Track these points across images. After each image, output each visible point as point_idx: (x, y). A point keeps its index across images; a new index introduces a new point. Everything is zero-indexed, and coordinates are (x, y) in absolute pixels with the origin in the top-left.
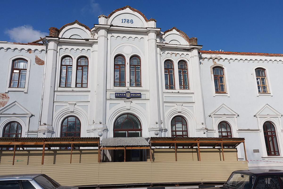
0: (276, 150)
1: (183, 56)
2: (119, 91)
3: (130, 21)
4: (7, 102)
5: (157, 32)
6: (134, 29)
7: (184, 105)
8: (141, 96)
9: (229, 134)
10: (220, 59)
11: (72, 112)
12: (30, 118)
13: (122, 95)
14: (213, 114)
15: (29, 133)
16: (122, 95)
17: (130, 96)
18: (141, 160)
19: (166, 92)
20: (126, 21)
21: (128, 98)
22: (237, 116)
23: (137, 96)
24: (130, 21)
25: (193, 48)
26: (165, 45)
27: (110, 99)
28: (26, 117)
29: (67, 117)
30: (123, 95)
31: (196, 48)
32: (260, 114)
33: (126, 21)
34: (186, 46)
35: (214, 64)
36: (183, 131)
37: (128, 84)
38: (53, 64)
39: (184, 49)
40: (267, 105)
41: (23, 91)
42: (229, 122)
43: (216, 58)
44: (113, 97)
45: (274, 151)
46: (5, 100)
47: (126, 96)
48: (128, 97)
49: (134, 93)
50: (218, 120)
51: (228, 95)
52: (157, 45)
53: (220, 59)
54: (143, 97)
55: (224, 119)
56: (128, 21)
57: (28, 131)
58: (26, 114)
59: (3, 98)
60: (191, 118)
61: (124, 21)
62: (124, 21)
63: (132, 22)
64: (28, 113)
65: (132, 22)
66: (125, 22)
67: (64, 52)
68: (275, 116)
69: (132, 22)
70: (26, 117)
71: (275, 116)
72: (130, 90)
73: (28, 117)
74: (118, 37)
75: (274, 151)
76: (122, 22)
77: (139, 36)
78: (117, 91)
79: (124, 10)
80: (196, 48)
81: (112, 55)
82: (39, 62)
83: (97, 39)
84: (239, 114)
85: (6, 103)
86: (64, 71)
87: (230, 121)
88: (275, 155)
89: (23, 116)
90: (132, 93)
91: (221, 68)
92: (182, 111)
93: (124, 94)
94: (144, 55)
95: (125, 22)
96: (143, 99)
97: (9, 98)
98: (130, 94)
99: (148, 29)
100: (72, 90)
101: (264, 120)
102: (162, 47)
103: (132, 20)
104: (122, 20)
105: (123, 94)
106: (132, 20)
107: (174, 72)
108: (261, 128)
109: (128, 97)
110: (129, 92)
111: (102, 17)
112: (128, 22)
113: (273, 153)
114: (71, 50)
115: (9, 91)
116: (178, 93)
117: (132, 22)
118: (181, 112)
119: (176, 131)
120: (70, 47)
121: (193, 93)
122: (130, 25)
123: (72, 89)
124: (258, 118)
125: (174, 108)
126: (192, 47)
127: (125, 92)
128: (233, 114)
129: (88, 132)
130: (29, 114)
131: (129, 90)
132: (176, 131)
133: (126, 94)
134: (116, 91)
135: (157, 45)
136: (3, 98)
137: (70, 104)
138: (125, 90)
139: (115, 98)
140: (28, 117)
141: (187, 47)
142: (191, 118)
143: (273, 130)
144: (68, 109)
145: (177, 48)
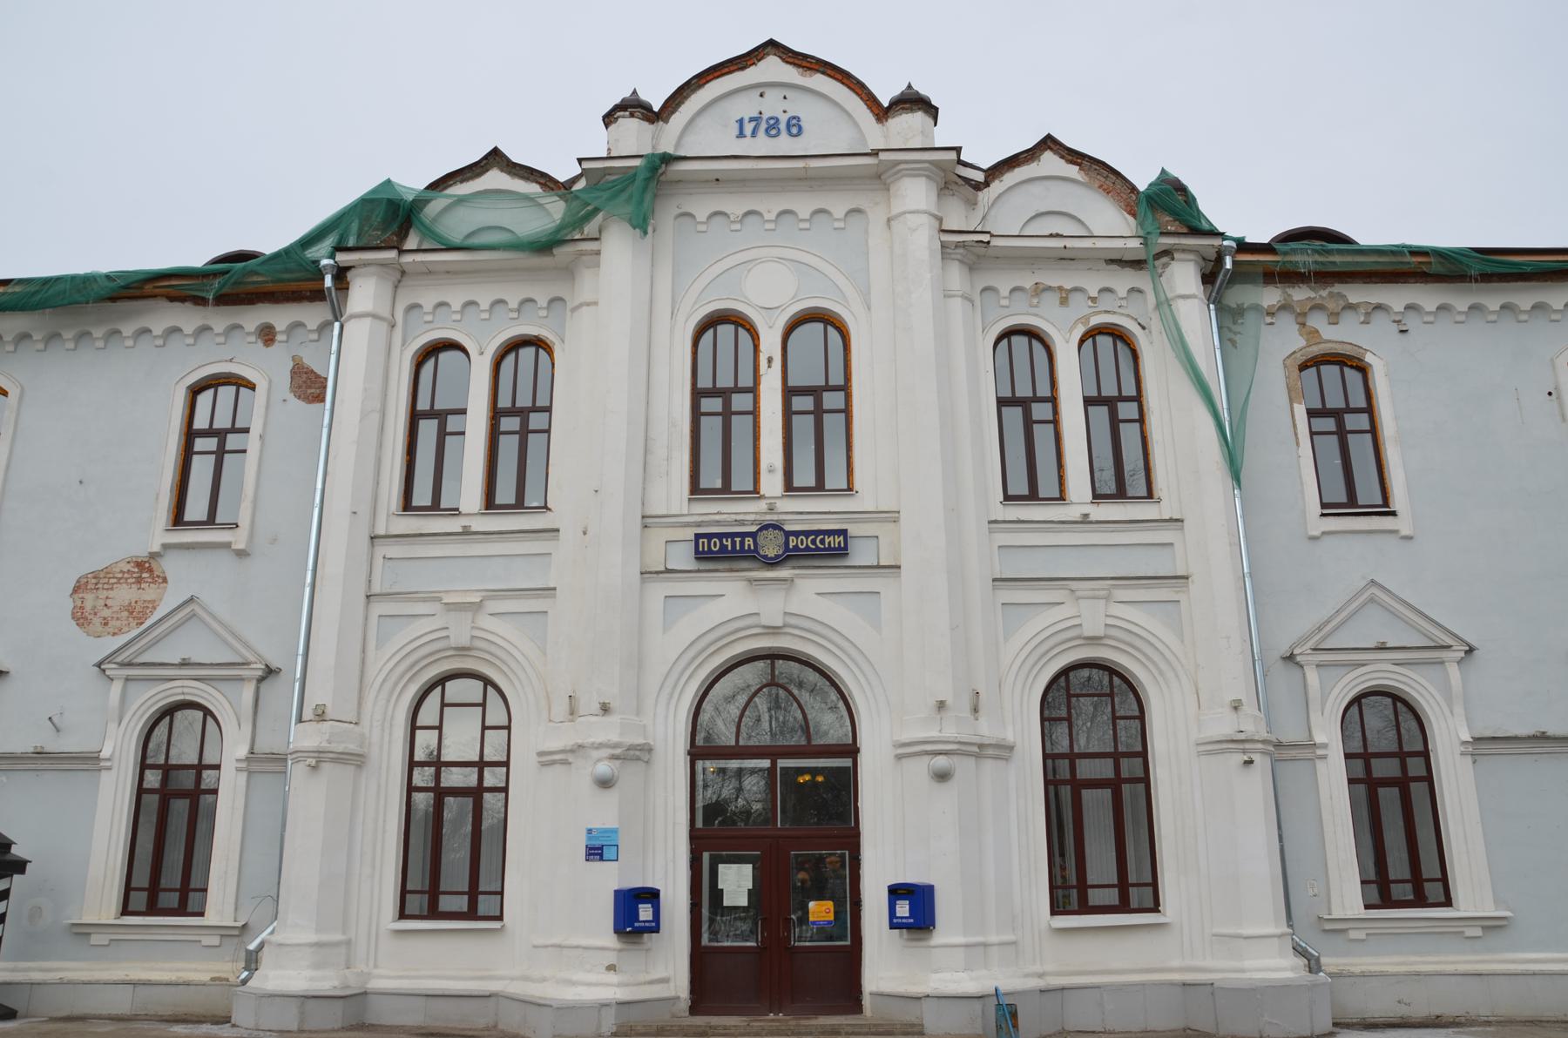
0: (1429, 869)
1: (1107, 302)
2: (718, 523)
3: (783, 126)
8: (846, 548)
11: (463, 651)
12: (264, 686)
13: (734, 543)
14: (1311, 644)
15: (255, 767)
16: (734, 543)
17: (781, 552)
18: (615, 929)
19: (1005, 522)
20: (763, 126)
22: (1462, 654)
24: (783, 126)
25: (1167, 253)
26: (988, 242)
27: (663, 569)
28: (241, 679)
30: (742, 543)
33: (763, 126)
34: (1119, 244)
35: (1307, 340)
36: (1116, 756)
37: (772, 484)
38: (365, 390)
41: (227, 545)
42: (1407, 689)
44: (683, 557)
45: (1417, 880)
46: (150, 592)
47: (756, 550)
48: (771, 558)
49: (807, 533)
51: (1402, 524)
52: (942, 247)
54: (861, 554)
55: (1381, 673)
56: (773, 128)
57: (252, 753)
59: (139, 580)
60: (1170, 675)
61: (748, 128)
62: (748, 128)
63: (795, 127)
65: (795, 131)
66: (754, 134)
67: (1006, 312)
68: (136, 647)
69: (795, 131)
70: (241, 679)
71: (136, 647)
73: (249, 679)
75: (1417, 880)
76: (741, 135)
78: (710, 523)
79: (748, 70)
83: (596, 239)
84: (1474, 643)
85: (153, 605)
86: (509, 446)
88: (1420, 900)
89: (226, 673)
90: (797, 534)
92: (1113, 632)
93: (749, 541)
94: (869, 309)
95: (754, 134)
96: (860, 567)
97: (165, 580)
98: (781, 539)
99: (882, 156)
101: (1347, 686)
102: (979, 257)
103: (794, 121)
104: (737, 125)
105: (738, 540)
106: (794, 121)
107: (630, 932)
109: (771, 553)
110: (776, 527)
111: (623, 117)
112: (773, 132)
113: (1403, 891)
114: (519, 310)
116: (1085, 520)
117: (795, 127)
120: (456, 298)
121: (1177, 520)
122: (784, 144)
123: (463, 521)
127: (754, 529)
128: (1433, 644)
129: (544, 764)
130: (252, 666)
133: (760, 540)
134: (699, 525)
135: (944, 246)
136: (139, 580)
138: (752, 517)
140: (249, 679)
141: (1129, 246)
142: (1170, 675)
143: (1128, 741)
144: (443, 633)
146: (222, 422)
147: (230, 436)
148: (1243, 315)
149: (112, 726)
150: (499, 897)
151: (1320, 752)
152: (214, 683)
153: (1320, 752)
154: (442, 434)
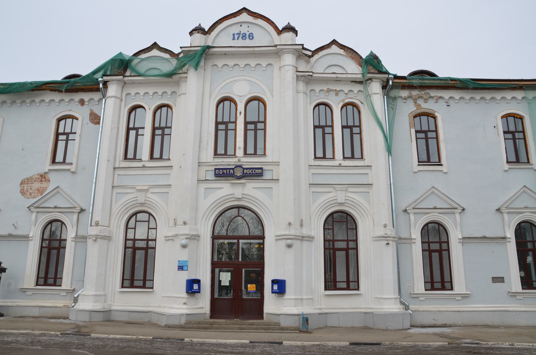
0: (447, 279)
1: (351, 95)
2: (222, 165)
3: (247, 36)
4: (47, 188)
5: (298, 52)
6: (251, 49)
7: (351, 189)
8: (262, 173)
9: (45, 243)
10: (429, 98)
13: (227, 172)
14: (412, 206)
16: (227, 172)
20: (241, 36)
21: (239, 178)
22: (461, 211)
23: (255, 174)
24: (247, 36)
28: (73, 212)
29: (135, 214)
30: (229, 171)
31: (376, 78)
32: (510, 206)
33: (241, 36)
34: (354, 76)
36: (348, 241)
37: (240, 152)
39: (353, 82)
40: (525, 189)
41: (69, 170)
43: (420, 97)
44: (211, 176)
46: (44, 185)
47: (234, 174)
48: (239, 177)
49: (250, 169)
50: (421, 220)
51: (444, 168)
53: (429, 98)
55: (435, 216)
58: (72, 208)
59: (41, 181)
61: (236, 37)
62: (236, 37)
64: (76, 206)
65: (251, 38)
66: (238, 39)
69: (251, 38)
70: (73, 212)
72: (242, 163)
74: (247, 66)
76: (234, 39)
77: (264, 62)
80: (376, 78)
81: (212, 99)
82: (96, 119)
85: (46, 189)
87: (446, 221)
89: (69, 210)
90: (247, 169)
91: (431, 115)
92: (347, 201)
95: (238, 39)
96: (266, 180)
97: (49, 181)
98: (242, 171)
100: (142, 166)
103: (251, 35)
104: (232, 36)
105: (228, 170)
106: (251, 35)
108: (511, 234)
109: (238, 175)
110: (240, 166)
111: (196, 33)
112: (244, 38)
115: (50, 170)
116: (340, 166)
118: (343, 203)
119: (334, 241)
121: (370, 166)
124: (506, 216)
125: (330, 195)
126: (369, 76)
127: (233, 167)
128: (452, 207)
129: (166, 240)
130: (77, 208)
131: (240, 163)
132: (334, 241)
134: (216, 165)
135: (297, 76)
136: (41, 181)
137: (138, 190)
139: (214, 178)
140: (76, 213)
143: (444, 239)
145: (337, 79)
146: (68, 130)
147: (229, 124)
148: (280, 57)
149: (33, 227)
150: (355, 251)
151: (413, 241)
152: (66, 214)
153: (413, 241)
154: (137, 135)
